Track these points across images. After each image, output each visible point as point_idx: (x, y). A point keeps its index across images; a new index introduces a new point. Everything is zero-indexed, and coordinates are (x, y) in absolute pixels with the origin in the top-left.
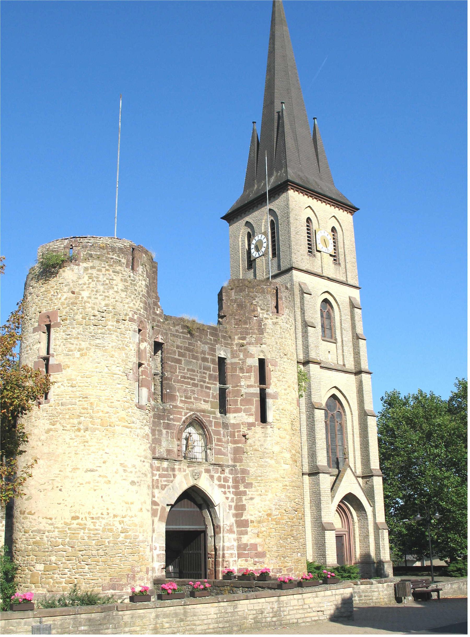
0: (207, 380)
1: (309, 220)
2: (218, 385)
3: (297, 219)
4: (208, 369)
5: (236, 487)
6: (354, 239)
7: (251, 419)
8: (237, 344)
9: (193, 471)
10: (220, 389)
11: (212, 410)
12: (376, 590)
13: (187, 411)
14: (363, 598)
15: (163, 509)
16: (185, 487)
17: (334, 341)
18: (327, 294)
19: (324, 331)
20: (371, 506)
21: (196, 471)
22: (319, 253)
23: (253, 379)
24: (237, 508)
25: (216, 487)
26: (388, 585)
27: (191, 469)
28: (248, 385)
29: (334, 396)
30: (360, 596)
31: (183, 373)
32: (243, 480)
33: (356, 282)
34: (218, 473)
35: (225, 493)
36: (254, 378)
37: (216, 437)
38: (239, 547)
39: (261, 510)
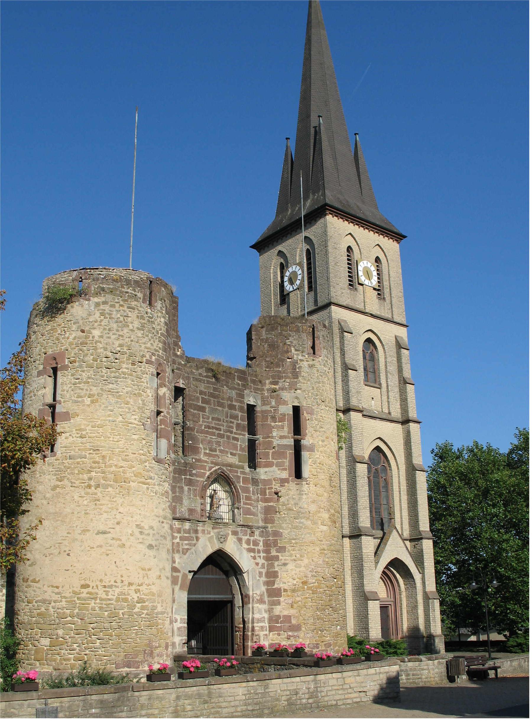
0: (234, 430)
1: (349, 249)
2: (247, 435)
3: (336, 248)
4: (236, 417)
7: (285, 475)
8: (268, 390)
10: (250, 440)
14: (411, 677)
15: (185, 576)
16: (210, 551)
17: (378, 386)
19: (367, 375)
20: (420, 573)
21: (221, 533)
22: (361, 287)
23: (286, 429)
25: (245, 553)
26: (439, 662)
27: (216, 531)
28: (281, 435)
29: (378, 449)
31: (208, 422)
32: (275, 543)
34: (246, 535)
35: (254, 558)
36: (287, 428)
37: (244, 495)
38: (270, 620)
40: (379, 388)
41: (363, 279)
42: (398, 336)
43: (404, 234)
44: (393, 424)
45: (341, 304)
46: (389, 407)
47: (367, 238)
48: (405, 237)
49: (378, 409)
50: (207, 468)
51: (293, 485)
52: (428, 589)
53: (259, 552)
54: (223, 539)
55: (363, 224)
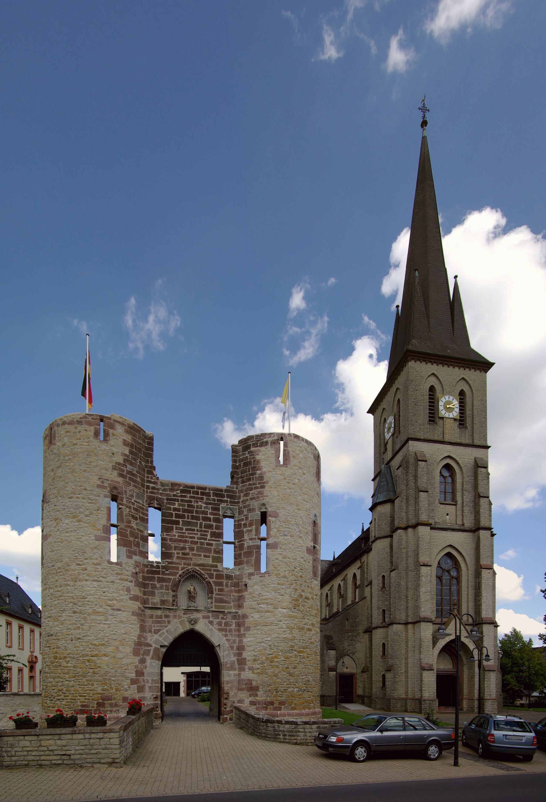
0: (209, 537)
3: (416, 390)
8: (242, 502)
11: (214, 563)
12: (301, 730)
21: (192, 617)
22: (441, 421)
25: (217, 631)
27: (187, 616)
29: (449, 555)
30: (285, 735)
31: (181, 533)
32: (243, 624)
35: (226, 636)
40: (456, 505)
41: (443, 412)
43: (491, 360)
44: (465, 534)
46: (463, 520)
50: (180, 569)
53: (230, 631)
55: (447, 361)
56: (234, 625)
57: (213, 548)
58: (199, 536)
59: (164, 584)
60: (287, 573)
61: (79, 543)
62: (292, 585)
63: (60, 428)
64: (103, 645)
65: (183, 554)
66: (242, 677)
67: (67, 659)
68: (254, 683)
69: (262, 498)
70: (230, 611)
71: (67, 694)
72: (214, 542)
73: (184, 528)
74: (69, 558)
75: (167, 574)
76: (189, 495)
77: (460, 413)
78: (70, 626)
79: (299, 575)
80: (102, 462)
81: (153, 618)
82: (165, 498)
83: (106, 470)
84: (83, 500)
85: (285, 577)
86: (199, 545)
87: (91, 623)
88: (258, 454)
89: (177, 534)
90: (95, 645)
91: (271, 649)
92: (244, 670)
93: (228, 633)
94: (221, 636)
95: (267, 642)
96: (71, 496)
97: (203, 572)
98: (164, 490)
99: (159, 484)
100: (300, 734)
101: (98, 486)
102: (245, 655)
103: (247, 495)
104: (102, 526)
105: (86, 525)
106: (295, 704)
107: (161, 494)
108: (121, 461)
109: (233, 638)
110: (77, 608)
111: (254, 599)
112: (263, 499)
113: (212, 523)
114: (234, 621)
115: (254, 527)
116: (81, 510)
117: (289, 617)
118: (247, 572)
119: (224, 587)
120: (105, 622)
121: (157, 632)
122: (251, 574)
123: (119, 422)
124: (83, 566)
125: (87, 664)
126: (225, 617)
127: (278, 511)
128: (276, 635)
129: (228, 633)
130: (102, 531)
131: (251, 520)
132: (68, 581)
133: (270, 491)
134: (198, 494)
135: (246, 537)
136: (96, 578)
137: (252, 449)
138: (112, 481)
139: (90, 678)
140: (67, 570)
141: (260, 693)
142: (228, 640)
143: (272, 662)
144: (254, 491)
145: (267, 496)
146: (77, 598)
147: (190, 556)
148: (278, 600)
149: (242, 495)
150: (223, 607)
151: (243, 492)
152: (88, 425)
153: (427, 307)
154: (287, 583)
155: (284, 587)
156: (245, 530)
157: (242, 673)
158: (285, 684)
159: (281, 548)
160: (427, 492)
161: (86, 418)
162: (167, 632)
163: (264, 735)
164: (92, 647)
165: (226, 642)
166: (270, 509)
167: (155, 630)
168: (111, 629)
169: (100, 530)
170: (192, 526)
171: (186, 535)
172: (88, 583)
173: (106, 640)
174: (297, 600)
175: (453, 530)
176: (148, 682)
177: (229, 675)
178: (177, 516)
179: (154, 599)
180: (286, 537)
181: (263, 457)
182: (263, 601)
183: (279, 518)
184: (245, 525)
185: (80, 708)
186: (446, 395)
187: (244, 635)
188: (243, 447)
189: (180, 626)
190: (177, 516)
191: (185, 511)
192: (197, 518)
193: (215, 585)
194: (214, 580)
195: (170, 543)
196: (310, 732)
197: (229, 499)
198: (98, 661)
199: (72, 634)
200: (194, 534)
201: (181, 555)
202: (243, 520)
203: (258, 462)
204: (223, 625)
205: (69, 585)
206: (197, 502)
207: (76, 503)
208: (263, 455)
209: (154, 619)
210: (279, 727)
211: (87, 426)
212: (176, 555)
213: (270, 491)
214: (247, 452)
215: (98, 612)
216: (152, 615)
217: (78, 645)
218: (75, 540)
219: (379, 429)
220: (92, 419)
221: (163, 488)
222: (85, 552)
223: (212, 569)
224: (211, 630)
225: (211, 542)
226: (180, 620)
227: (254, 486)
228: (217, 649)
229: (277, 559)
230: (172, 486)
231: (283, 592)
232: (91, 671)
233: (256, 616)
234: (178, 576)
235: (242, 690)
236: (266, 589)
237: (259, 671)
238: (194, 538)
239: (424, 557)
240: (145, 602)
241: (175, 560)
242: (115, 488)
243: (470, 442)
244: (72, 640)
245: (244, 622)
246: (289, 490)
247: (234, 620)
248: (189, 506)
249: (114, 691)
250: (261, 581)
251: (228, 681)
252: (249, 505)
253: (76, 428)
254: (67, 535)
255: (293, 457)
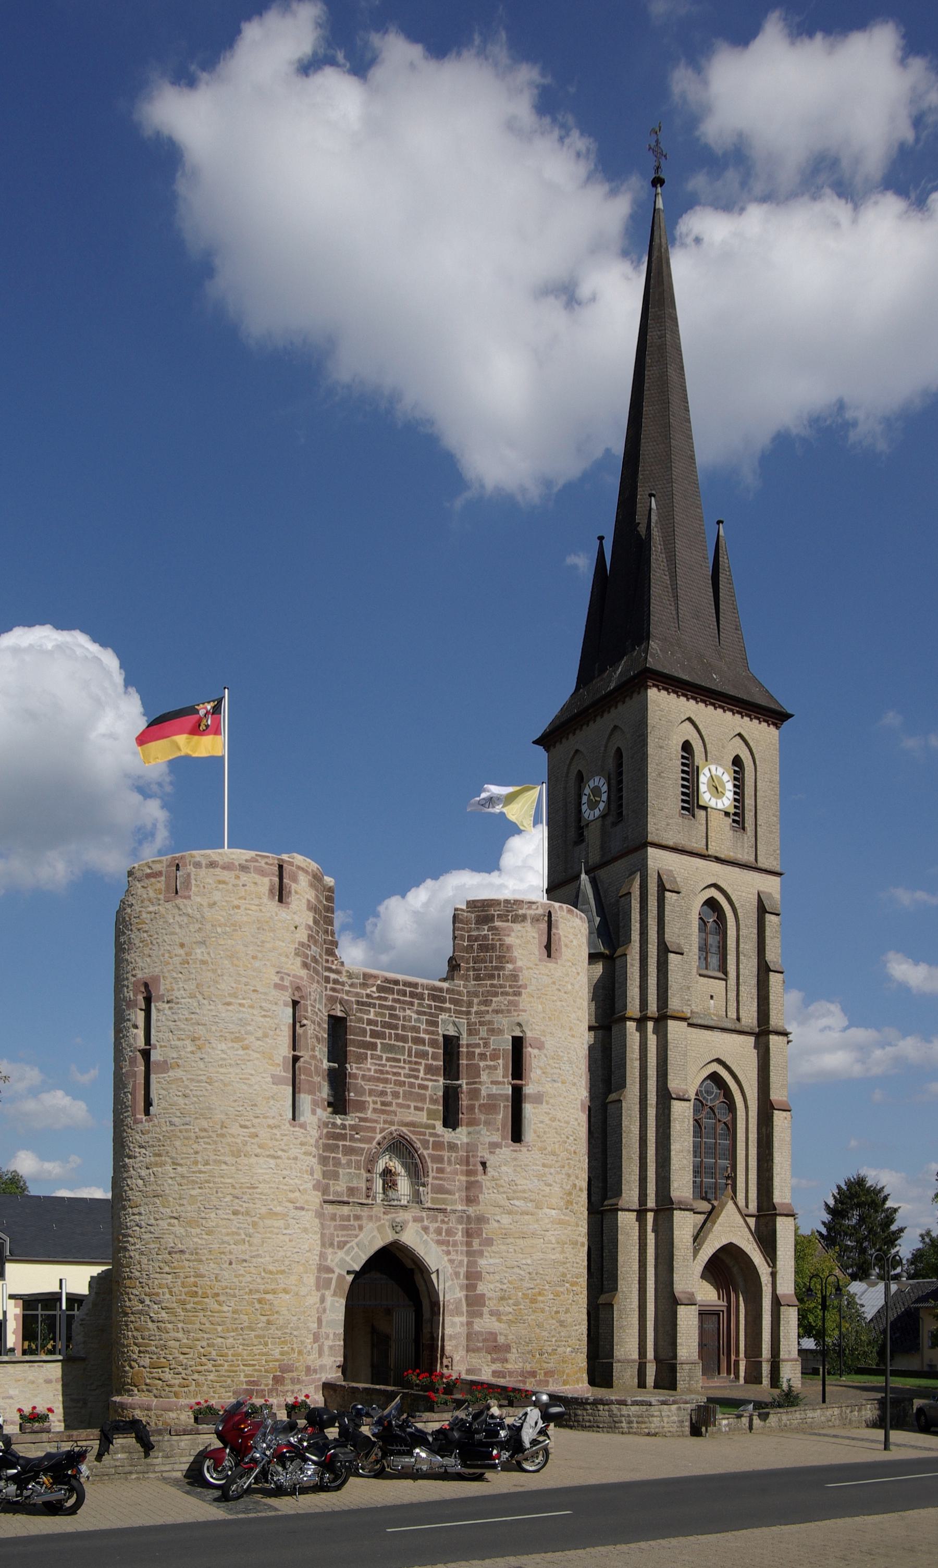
0: (421, 1074)
1: (687, 747)
2: (441, 1080)
3: (661, 747)
4: (424, 1055)
5: (469, 1244)
6: (777, 778)
7: (496, 1138)
8: (477, 1013)
9: (393, 1220)
10: (447, 1089)
12: (656, 1414)
13: (386, 1126)
14: (635, 1425)
15: (340, 1277)
16: (379, 1244)
17: (724, 977)
18: (713, 889)
19: (706, 959)
20: (769, 1266)
22: (703, 813)
23: (500, 1071)
24: (468, 1276)
25: (434, 1246)
26: (679, 1409)
28: (493, 1082)
30: (630, 1422)
31: (379, 1065)
32: (479, 1233)
33: (775, 863)
34: (437, 1222)
35: (448, 1253)
36: (503, 1066)
37: (435, 1166)
38: (469, 1336)
39: (506, 1281)
40: (726, 980)
41: (706, 796)
42: (763, 892)
43: (790, 712)
45: (664, 843)
47: (720, 724)
48: (789, 716)
49: (721, 1013)
50: (378, 1131)
51: (507, 1151)
52: (780, 1291)
53: (455, 1244)
54: (397, 1227)
56: (460, 1234)
57: (428, 1093)
58: (407, 1071)
59: (353, 1158)
60: (557, 1146)
61: (245, 1087)
62: (564, 1167)
63: (203, 872)
64: (282, 1272)
65: (383, 1104)
66: (476, 1328)
67: (222, 1298)
68: (501, 1340)
69: (516, 1014)
70: (454, 1208)
71: (219, 1362)
72: (430, 1084)
73: (384, 1056)
74: (227, 1114)
75: (357, 1139)
76: (391, 997)
77: (735, 800)
78: (226, 1238)
79: (572, 1149)
80: (281, 943)
81: (335, 1220)
82: (353, 999)
83: (287, 956)
84: (250, 1010)
85: (553, 1153)
86: (406, 1088)
87: (266, 1233)
88: (509, 935)
89: (373, 1068)
90: (271, 1272)
91: (531, 1279)
92: (481, 1315)
93: (450, 1248)
94: (441, 1253)
95: (525, 1267)
96: (228, 1000)
97: (413, 1137)
98: (352, 985)
99: (344, 974)
100: (655, 1419)
101: (277, 986)
102: (482, 1288)
103: (486, 1003)
104: (281, 1059)
105: (258, 1056)
106: (568, 1374)
107: (348, 993)
108: (305, 941)
109: (459, 1258)
110: (241, 1206)
111: (501, 1190)
112: (518, 1015)
113: (427, 1048)
114: (460, 1227)
115: (500, 1061)
116: (249, 1028)
117: (559, 1223)
118: (487, 1140)
119: (446, 1165)
120: (285, 1232)
121: (342, 1245)
122: (494, 1146)
123: (302, 869)
124: (253, 1130)
125: (257, 1306)
126: (446, 1219)
127: (543, 1039)
128: (541, 1256)
129: (450, 1248)
130: (281, 1068)
131: (494, 1050)
132: (224, 1154)
133: (530, 1002)
134: (405, 995)
135: (484, 1077)
136: (272, 1152)
137: (497, 924)
138: (295, 976)
139: (261, 1333)
140: (223, 1136)
141: (512, 1356)
142: (451, 1261)
143: (534, 1301)
144: (499, 998)
145: (525, 1011)
146: (241, 1188)
147: (394, 1108)
148: (542, 1193)
149: (476, 1000)
150: (444, 1201)
151: (478, 997)
152: (259, 874)
153: (673, 576)
154: (557, 1165)
155: (552, 1170)
156: (482, 1064)
157: (477, 1320)
158: (554, 1340)
159: (548, 1103)
160: (682, 954)
161: (257, 861)
162: (357, 1245)
163: (588, 1424)
164: (267, 1276)
165: (448, 1265)
166: (529, 1034)
167: (339, 1242)
168: (294, 1243)
169: (279, 1065)
170: (396, 1053)
171: (388, 1068)
172: (261, 1160)
173: (287, 1263)
174: (570, 1194)
175: (724, 1030)
176: (327, 1337)
177: (453, 1324)
178: (374, 1034)
179: (338, 1185)
180: (556, 1085)
181: (518, 941)
182: (518, 1194)
183: (545, 1051)
184: (483, 1056)
185: (245, 1387)
186: (712, 764)
187: (481, 1253)
188: (478, 916)
189: (378, 1235)
190: (374, 1034)
191: (386, 1025)
192: (404, 1039)
193: (432, 1162)
194: (430, 1151)
195: (363, 1083)
196: (668, 1416)
197: (452, 1007)
198: (275, 1303)
199: (231, 1253)
200: (400, 1067)
201: (379, 1106)
202: (478, 1045)
203: (509, 948)
204: (444, 1234)
205: (225, 1163)
206: (404, 1010)
207: (241, 1016)
208: (518, 937)
209: (338, 1223)
210: (620, 1410)
211: (257, 876)
212: (372, 1105)
213: (530, 1002)
214: (486, 927)
215: (276, 1214)
216: (335, 1215)
217: (242, 1272)
218: (238, 1082)
219: (565, 788)
220: (266, 863)
221: (350, 982)
222: (255, 1105)
223: (427, 1131)
224: (426, 1242)
225: (426, 1083)
226: (379, 1223)
227: (500, 990)
228: (434, 1277)
229: (542, 1122)
230: (364, 979)
231: (550, 1179)
232: (264, 1319)
233: (506, 1220)
234: (374, 1143)
235: (477, 1350)
236: (524, 1174)
237: (510, 1317)
238: (399, 1074)
239: (677, 1082)
240: (325, 1191)
241: (369, 1114)
242: (298, 988)
243: (748, 858)
244: (231, 1264)
245: (481, 1229)
246: (559, 1003)
247: (461, 1224)
248: (391, 1016)
249: (296, 1355)
250: (515, 1159)
251: (451, 1335)
252: (491, 1023)
253: (238, 877)
254: (222, 1070)
255: (566, 946)
